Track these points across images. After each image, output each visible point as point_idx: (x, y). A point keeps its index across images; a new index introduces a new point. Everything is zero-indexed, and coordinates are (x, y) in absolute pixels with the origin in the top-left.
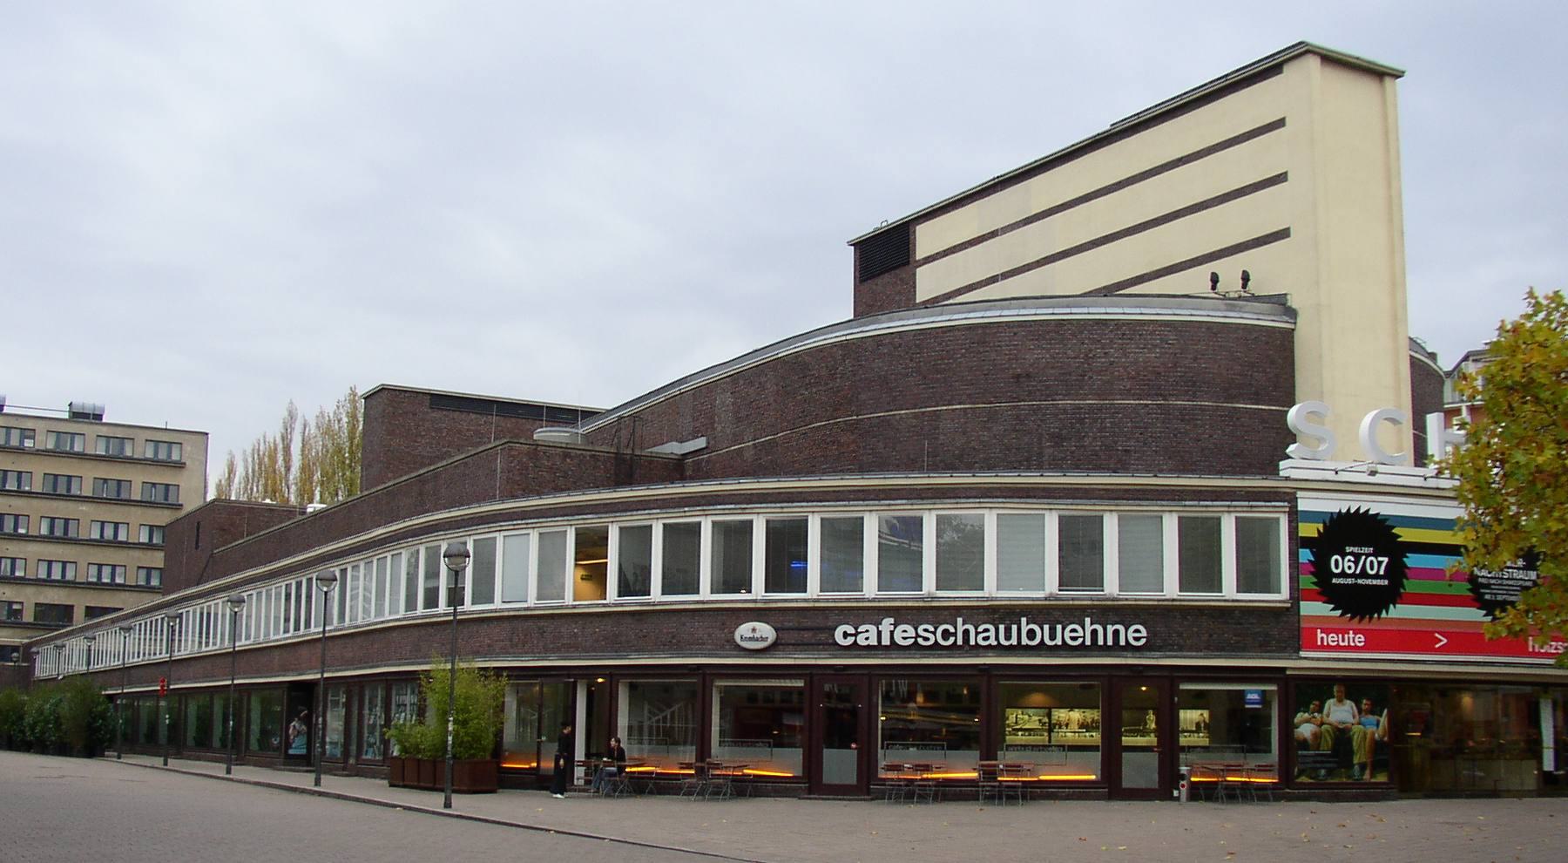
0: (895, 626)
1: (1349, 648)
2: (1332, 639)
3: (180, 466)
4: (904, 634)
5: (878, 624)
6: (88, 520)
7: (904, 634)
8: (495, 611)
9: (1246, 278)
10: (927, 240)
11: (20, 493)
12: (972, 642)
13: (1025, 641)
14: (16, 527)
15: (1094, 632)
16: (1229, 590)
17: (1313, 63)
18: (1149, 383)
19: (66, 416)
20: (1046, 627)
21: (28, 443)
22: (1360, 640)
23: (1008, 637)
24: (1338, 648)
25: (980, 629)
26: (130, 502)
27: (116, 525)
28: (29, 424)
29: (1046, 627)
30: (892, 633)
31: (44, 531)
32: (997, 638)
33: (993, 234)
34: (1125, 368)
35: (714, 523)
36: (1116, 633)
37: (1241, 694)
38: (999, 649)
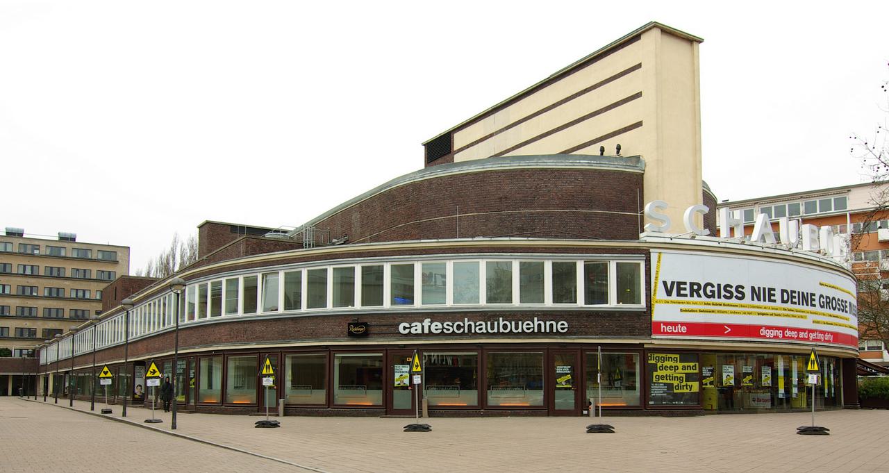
0: (431, 322)
1: (678, 333)
2: (669, 329)
3: (116, 262)
4: (436, 327)
5: (422, 322)
6: (69, 288)
7: (436, 327)
8: (208, 321)
9: (619, 148)
10: (459, 140)
11: (32, 276)
12: (473, 331)
13: (502, 330)
14: (31, 293)
15: (539, 325)
16: (613, 303)
17: (656, 33)
18: (569, 201)
19: (57, 239)
20: (513, 323)
21: (36, 252)
22: (763, 332)
23: (492, 328)
24: (672, 333)
25: (477, 324)
26: (90, 280)
27: (84, 291)
28: (36, 243)
29: (513, 323)
30: (430, 326)
31: (46, 294)
32: (486, 329)
33: (491, 135)
34: (556, 193)
35: (334, 269)
36: (551, 325)
37: (763, 357)
38: (488, 335)
